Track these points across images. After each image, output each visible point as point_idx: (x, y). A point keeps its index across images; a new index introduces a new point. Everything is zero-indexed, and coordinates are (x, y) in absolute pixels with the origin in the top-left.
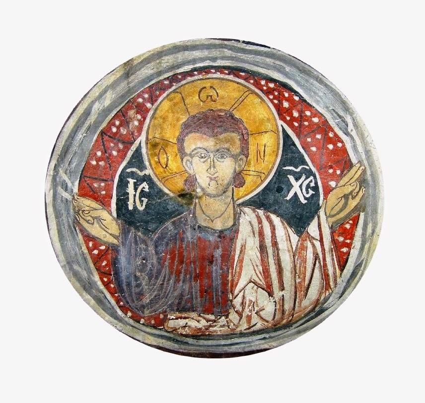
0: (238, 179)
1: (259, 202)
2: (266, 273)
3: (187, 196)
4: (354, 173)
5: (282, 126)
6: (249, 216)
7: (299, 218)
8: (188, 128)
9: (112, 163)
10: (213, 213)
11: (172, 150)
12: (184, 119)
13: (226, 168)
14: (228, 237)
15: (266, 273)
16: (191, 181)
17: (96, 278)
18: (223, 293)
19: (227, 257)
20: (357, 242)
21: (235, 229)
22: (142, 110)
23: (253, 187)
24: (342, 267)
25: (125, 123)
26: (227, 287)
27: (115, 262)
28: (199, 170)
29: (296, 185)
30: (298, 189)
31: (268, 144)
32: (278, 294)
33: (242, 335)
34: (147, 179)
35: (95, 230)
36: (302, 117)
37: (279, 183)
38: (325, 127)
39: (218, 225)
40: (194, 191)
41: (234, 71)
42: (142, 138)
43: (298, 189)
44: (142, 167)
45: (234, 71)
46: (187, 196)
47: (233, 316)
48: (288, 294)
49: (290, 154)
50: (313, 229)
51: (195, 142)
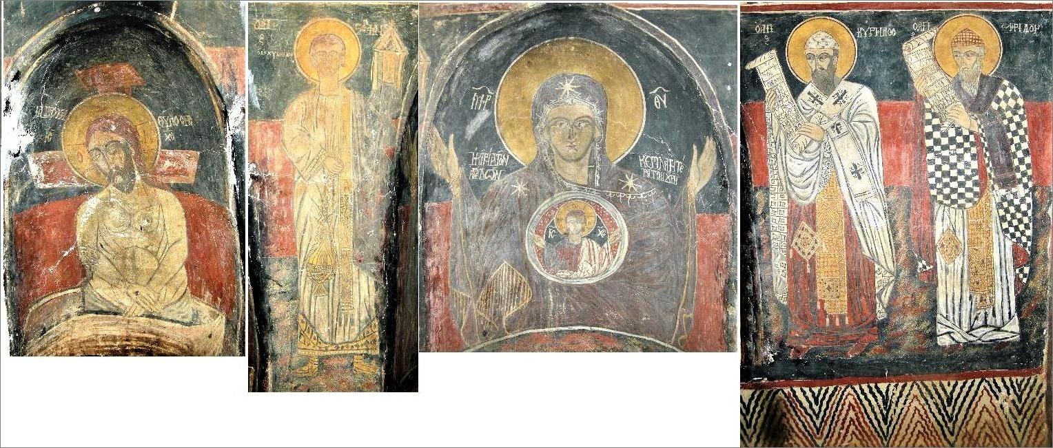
0: (583, 230)
1: (588, 237)
2: (590, 259)
3: (567, 234)
4: (618, 230)
5: (1020, 431)
6: (585, 241)
7: (601, 242)
8: (568, 215)
9: (545, 224)
10: (574, 240)
11: (563, 222)
12: (568, 212)
13: (579, 226)
14: (579, 247)
15: (590, 259)
16: (568, 230)
17: (537, 258)
18: (147, 342)
19: (578, 253)
20: (619, 250)
21: (581, 244)
22: (555, 209)
23: (587, 233)
24: (614, 257)
25: (550, 213)
26: (577, 262)
27: (543, 254)
28: (572, 228)
29: (600, 232)
30: (601, 233)
31: (592, 221)
32: (594, 265)
33: (582, 278)
34: (555, 229)
35: (538, 244)
36: (603, 213)
37: (595, 231)
38: (610, 216)
39: (576, 243)
40: (496, 222)
41: (584, 200)
42: (554, 218)
43: (601, 233)
44: (554, 225)
45: (584, 200)
46: (567, 234)
47: (579, 272)
48: (597, 266)
49: (599, 223)
50: (605, 245)
51: (572, 219)
